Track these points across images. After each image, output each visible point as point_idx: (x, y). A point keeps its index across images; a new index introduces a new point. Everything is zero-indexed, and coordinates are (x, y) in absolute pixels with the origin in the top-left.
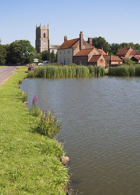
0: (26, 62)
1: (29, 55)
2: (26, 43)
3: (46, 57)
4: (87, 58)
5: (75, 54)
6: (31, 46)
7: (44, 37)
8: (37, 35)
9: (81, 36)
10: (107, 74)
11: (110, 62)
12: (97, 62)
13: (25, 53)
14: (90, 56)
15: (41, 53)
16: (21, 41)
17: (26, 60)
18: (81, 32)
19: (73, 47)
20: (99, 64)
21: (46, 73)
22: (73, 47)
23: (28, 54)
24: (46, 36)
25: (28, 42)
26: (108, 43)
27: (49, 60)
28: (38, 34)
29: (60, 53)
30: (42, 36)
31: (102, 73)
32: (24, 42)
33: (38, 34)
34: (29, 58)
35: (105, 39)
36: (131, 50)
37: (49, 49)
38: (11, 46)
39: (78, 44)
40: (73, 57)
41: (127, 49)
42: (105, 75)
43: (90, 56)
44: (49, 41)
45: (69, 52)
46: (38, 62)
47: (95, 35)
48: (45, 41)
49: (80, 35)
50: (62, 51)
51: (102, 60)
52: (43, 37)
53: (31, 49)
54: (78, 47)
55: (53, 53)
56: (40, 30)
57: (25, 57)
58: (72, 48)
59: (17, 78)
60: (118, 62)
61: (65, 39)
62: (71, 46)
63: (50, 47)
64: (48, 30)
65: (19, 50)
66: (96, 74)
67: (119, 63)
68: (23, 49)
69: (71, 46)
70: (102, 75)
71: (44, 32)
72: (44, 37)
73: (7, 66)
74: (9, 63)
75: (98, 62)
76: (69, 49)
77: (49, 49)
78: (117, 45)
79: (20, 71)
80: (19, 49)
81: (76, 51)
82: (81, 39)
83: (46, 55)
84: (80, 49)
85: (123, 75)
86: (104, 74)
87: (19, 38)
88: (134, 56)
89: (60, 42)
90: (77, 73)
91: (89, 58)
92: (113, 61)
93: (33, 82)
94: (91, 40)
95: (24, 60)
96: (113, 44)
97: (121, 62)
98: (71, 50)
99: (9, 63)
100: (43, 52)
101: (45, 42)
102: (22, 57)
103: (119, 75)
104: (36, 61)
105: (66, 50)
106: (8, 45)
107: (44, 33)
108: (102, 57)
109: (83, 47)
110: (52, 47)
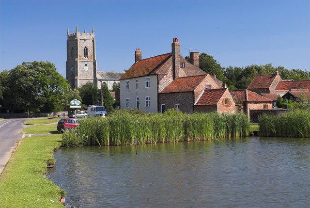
0: (45, 109)
1: (53, 94)
2: (48, 68)
3: (90, 96)
4: (190, 96)
5: (162, 88)
6: (57, 74)
7: (86, 54)
8: (70, 52)
9: (176, 47)
10: (254, 132)
11: (245, 104)
12: (216, 106)
13: (43, 89)
14: (200, 91)
15: (79, 89)
16: (35, 64)
17: (46, 104)
18: (175, 40)
19: (158, 72)
20: (221, 109)
21: (110, 133)
22: (157, 73)
23: (51, 92)
24: (90, 53)
25: (50, 66)
26: (219, 65)
27: (100, 104)
28: (72, 50)
29: (127, 87)
30: (80, 52)
31: (244, 132)
32: (41, 66)
33: (72, 50)
34: (53, 100)
35: (214, 58)
36: (278, 78)
37: (95, 80)
38: (12, 76)
39: (168, 67)
40: (159, 95)
41: (271, 77)
42: (251, 135)
43: (200, 91)
44: (94, 63)
45: (148, 84)
46: (80, 107)
47: (200, 49)
48: (87, 63)
49: (173, 45)
50: (133, 82)
51: (227, 101)
52: (83, 55)
53: (57, 81)
54: (170, 73)
55: (105, 87)
56: (77, 40)
57: (44, 98)
58: (155, 74)
59: (37, 152)
60: (263, 104)
61: (137, 58)
62: (154, 70)
63: (98, 77)
64: (93, 41)
65: (30, 83)
66: (228, 132)
67: (265, 106)
68: (41, 81)
69: (154, 70)
70: (244, 136)
71: (85, 45)
72: (86, 54)
73: (3, 119)
74: (8, 111)
75: (219, 104)
76: (148, 77)
77: (95, 80)
78: (238, 70)
79: (34, 135)
80: (31, 80)
81: (166, 82)
82: (176, 56)
83: (90, 93)
84: (174, 77)
85: (298, 136)
86: (247, 134)
87: (30, 59)
88: (290, 91)
89: (126, 64)
90: (186, 133)
91: (198, 94)
92: (251, 102)
93: (82, 160)
94: (196, 57)
95: (42, 104)
96: (230, 70)
97: (268, 104)
98: (153, 79)
99: (8, 111)
100: (84, 86)
101: (86, 65)
102: (36, 98)
103: (286, 136)
104: (75, 105)
105: (140, 79)
106: (5, 72)
107: (84, 47)
108: (227, 94)
109: (181, 73)
110: (102, 75)
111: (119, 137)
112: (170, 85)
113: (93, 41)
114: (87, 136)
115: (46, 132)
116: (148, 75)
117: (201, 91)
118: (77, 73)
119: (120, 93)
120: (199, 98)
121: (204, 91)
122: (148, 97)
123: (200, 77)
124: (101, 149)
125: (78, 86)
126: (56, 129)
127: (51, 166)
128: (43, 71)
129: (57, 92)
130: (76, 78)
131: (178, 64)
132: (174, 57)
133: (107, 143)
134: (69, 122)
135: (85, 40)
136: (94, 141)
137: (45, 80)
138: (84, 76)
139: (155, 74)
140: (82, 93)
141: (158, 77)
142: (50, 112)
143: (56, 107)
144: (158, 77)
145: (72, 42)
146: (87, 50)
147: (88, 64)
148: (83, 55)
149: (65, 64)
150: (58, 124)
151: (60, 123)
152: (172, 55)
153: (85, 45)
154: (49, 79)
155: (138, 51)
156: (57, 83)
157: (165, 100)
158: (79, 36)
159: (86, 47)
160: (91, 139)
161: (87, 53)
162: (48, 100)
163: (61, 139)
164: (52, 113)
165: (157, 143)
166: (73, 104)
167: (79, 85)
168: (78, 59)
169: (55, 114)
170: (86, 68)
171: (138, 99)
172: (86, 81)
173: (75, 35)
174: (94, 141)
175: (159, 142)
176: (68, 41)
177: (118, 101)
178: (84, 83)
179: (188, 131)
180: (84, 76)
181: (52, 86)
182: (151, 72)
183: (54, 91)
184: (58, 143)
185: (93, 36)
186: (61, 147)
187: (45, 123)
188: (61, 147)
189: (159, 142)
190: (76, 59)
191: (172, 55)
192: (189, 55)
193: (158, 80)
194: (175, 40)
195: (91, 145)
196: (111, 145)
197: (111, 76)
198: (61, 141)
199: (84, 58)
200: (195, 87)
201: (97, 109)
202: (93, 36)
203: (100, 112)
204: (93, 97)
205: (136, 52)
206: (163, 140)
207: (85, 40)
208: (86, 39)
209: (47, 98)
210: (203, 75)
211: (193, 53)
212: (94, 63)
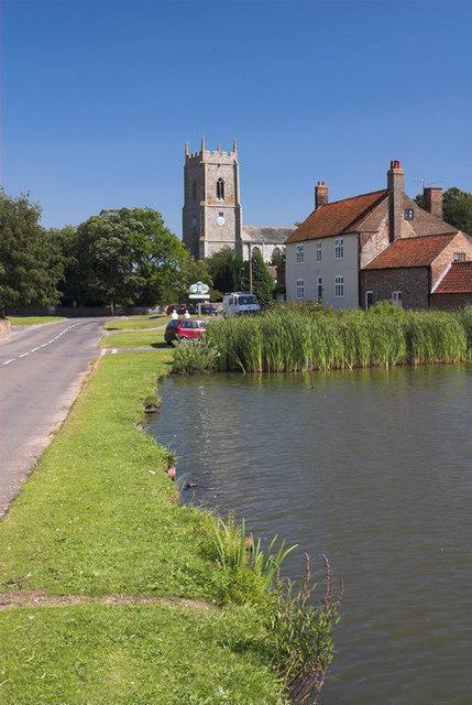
3: (228, 275)
5: (368, 259)
6: (166, 231)
7: (220, 193)
18: (395, 164)
19: (360, 227)
24: (228, 189)
25: (152, 216)
29: (300, 257)
34: (158, 282)
37: (239, 243)
44: (237, 211)
45: (340, 252)
48: (221, 210)
49: (390, 175)
53: (166, 246)
54: (383, 229)
55: (257, 257)
62: (352, 224)
63: (245, 237)
64: (235, 167)
69: (352, 224)
72: (220, 193)
77: (239, 243)
81: (376, 247)
82: (397, 195)
89: (299, 211)
90: (410, 347)
101: (221, 214)
109: (406, 229)
110: (251, 234)
112: (384, 253)
113: (235, 167)
115: (143, 343)
117: (445, 266)
120: (438, 283)
121: (450, 266)
123: (443, 237)
127: (153, 409)
128: (138, 228)
129: (166, 267)
131: (399, 213)
135: (219, 165)
136: (233, 364)
138: (217, 236)
142: (152, 304)
145: (194, 172)
147: (226, 211)
148: (215, 194)
152: (388, 194)
153: (219, 175)
154: (149, 242)
156: (166, 249)
157: (374, 284)
158: (207, 157)
159: (220, 179)
163: (172, 359)
166: (195, 291)
167: (207, 254)
168: (206, 203)
170: (221, 221)
171: (320, 280)
172: (222, 246)
173: (201, 157)
174: (233, 364)
175: (358, 367)
178: (218, 248)
180: (217, 236)
182: (345, 229)
185: (234, 156)
189: (358, 367)
191: (388, 194)
194: (395, 164)
195: (228, 370)
196: (265, 371)
200: (433, 258)
201: (241, 301)
202: (234, 156)
205: (316, 189)
206: (365, 362)
207: (219, 165)
212: (237, 211)
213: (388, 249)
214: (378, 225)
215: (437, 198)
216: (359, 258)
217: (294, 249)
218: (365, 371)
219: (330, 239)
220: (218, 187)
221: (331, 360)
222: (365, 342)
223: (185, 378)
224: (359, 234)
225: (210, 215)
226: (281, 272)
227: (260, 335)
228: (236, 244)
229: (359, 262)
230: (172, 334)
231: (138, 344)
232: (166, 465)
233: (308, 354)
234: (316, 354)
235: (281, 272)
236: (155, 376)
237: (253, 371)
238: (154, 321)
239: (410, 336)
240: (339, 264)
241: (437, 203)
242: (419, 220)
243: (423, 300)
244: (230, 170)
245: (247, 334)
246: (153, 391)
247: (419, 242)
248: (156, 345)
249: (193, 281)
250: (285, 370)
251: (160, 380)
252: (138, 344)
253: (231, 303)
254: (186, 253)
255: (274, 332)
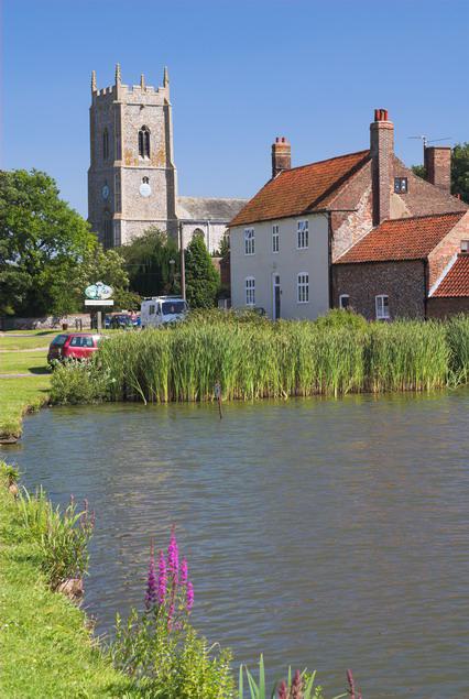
1: (52, 263)
2: (34, 190)
3: (155, 272)
5: (342, 249)
6: (61, 207)
7: (144, 147)
9: (381, 134)
13: (22, 250)
15: (126, 251)
18: (380, 114)
19: (330, 205)
23: (45, 258)
24: (156, 142)
25: (41, 182)
28: (106, 136)
29: (250, 248)
30: (129, 142)
32: (16, 184)
33: (106, 136)
34: (50, 282)
37: (174, 226)
44: (170, 174)
45: (303, 239)
46: (111, 303)
48: (146, 173)
49: (374, 129)
50: (263, 233)
53: (62, 229)
54: (364, 207)
55: (197, 247)
58: (323, 211)
61: (278, 164)
62: (321, 199)
63: (181, 213)
64: (166, 109)
69: (321, 199)
72: (144, 147)
76: (303, 220)
77: (174, 226)
81: (353, 233)
82: (383, 159)
89: (247, 181)
90: (367, 370)
91: (439, 266)
95: (19, 293)
98: (317, 224)
100: (138, 242)
101: (146, 180)
104: (98, 298)
107: (138, 127)
109: (396, 207)
110: (192, 209)
111: (192, 379)
112: (366, 240)
113: (166, 109)
114: (114, 380)
115: (18, 368)
116: (305, 214)
117: (449, 258)
118: (119, 203)
119: (232, 262)
120: (441, 278)
121: (455, 258)
122: (252, 278)
123: (446, 218)
124: (147, 407)
125: (123, 241)
126: (44, 363)
127: (12, 440)
128: (18, 201)
129: (62, 259)
130: (116, 216)
131: (387, 183)
132: (378, 161)
133: (162, 394)
134: (78, 344)
135: (142, 107)
136: (133, 388)
137: (25, 224)
138: (140, 212)
139: (323, 211)
140: (133, 261)
141: (330, 219)
142: (42, 315)
143: (60, 301)
144: (330, 219)
145: (105, 114)
146: (147, 134)
147: (152, 176)
148: (135, 149)
149: (87, 175)
150: (51, 348)
151: (54, 346)
152: (371, 157)
153: (143, 122)
154: (37, 221)
155: (280, 143)
156: (62, 233)
157: (354, 284)
158: (124, 95)
159: (144, 128)
160: (124, 387)
161: (148, 144)
162: (35, 282)
163: (49, 386)
164: (50, 319)
165: (290, 396)
166: (93, 294)
167: (125, 240)
168: (122, 163)
169: (56, 322)
170: (146, 189)
171: (278, 278)
172: (146, 227)
173: (114, 94)
174: (133, 388)
175: (296, 395)
176: (92, 110)
177: (225, 287)
178: (140, 231)
179: (374, 367)
180: (140, 212)
181: (48, 241)
182: (311, 207)
183: (54, 255)
184: (40, 394)
185: (164, 94)
186: (49, 403)
187: (23, 348)
188: (49, 403)
189: (296, 395)
190: (116, 163)
191: (371, 157)
192: (420, 162)
193: (330, 225)
194: (380, 114)
195: (125, 399)
196: (172, 400)
197: (217, 208)
198: (48, 391)
199: (140, 158)
200: (431, 247)
201: (167, 308)
202: (164, 94)
203: (175, 315)
204: (164, 272)
205: (274, 147)
206: (306, 388)
207: (142, 107)
208: (144, 103)
209: (33, 275)
210: (458, 213)
211: (433, 149)
212: (170, 174)
213: (371, 234)
214: (357, 200)
215: (443, 162)
216: (330, 249)
217: (240, 236)
218: (307, 402)
219: (267, 224)
220: (141, 139)
221: (261, 386)
222: (309, 363)
223: (65, 408)
224: (330, 213)
225: (128, 180)
226: (226, 265)
227: (166, 357)
228: (169, 223)
229: (330, 253)
230: (59, 351)
231: (9, 369)
232: (7, 480)
233: (230, 382)
234: (240, 379)
235: (226, 265)
236: (24, 406)
237: (155, 400)
238: (41, 338)
239: (369, 355)
240: (300, 256)
241: (443, 168)
242: (416, 193)
243: (418, 306)
244: (159, 112)
245: (155, 351)
246: (17, 421)
247: (414, 224)
248: (36, 371)
249: (93, 280)
250: (198, 399)
251: (31, 411)
252: (9, 369)
253: (152, 312)
254: (93, 237)
255: (189, 348)
